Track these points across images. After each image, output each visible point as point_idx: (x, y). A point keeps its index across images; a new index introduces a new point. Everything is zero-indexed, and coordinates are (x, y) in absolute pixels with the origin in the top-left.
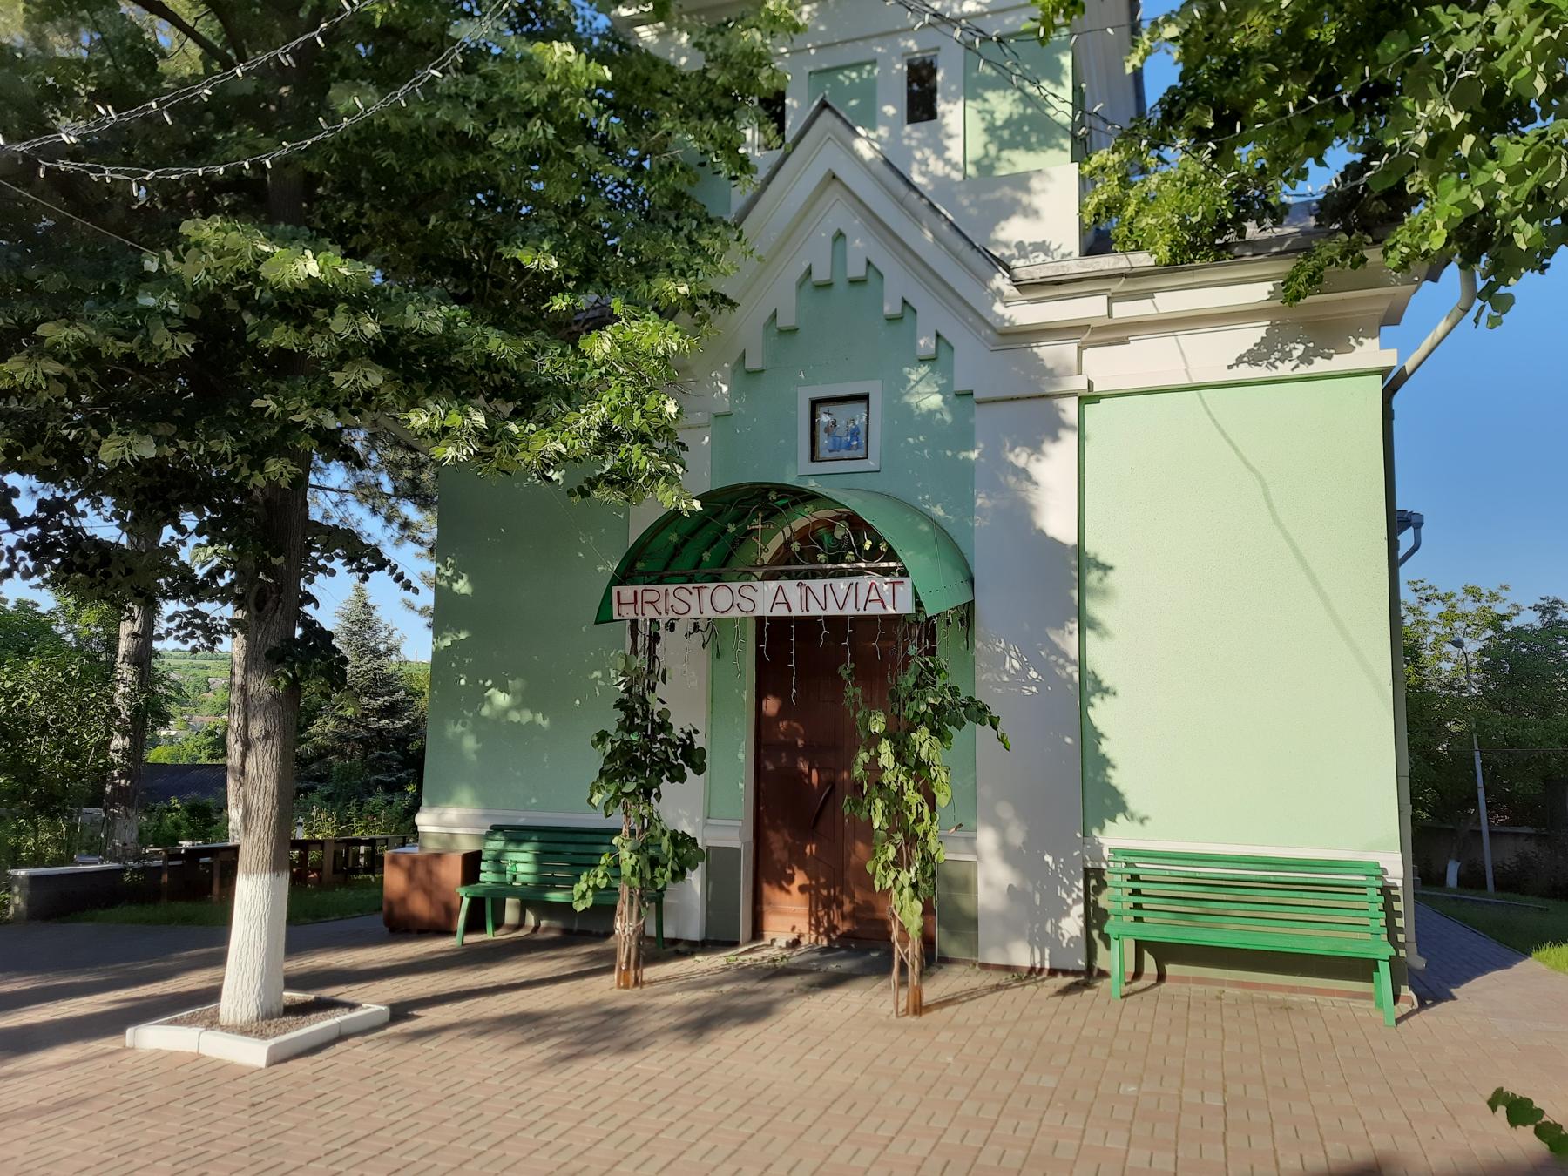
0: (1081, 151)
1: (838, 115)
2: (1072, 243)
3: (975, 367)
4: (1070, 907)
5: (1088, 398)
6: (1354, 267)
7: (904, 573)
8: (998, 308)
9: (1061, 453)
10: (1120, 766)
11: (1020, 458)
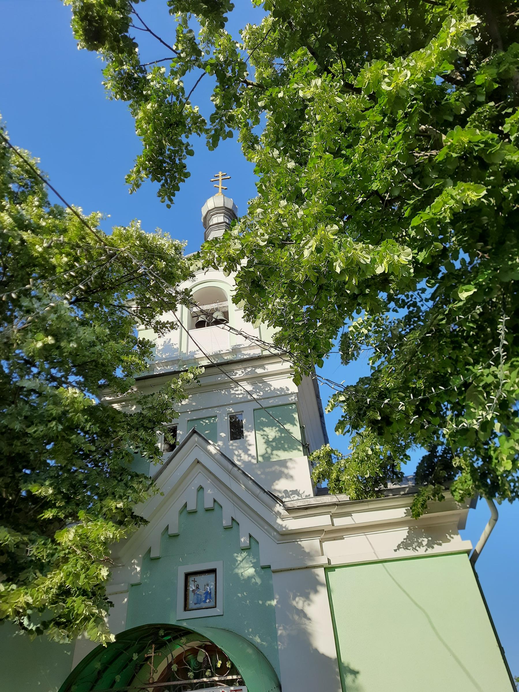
0: (307, 450)
1: (200, 436)
2: (309, 490)
3: (271, 553)
5: (329, 568)
6: (440, 500)
7: (242, 683)
8: (279, 521)
9: (320, 598)
11: (299, 603)
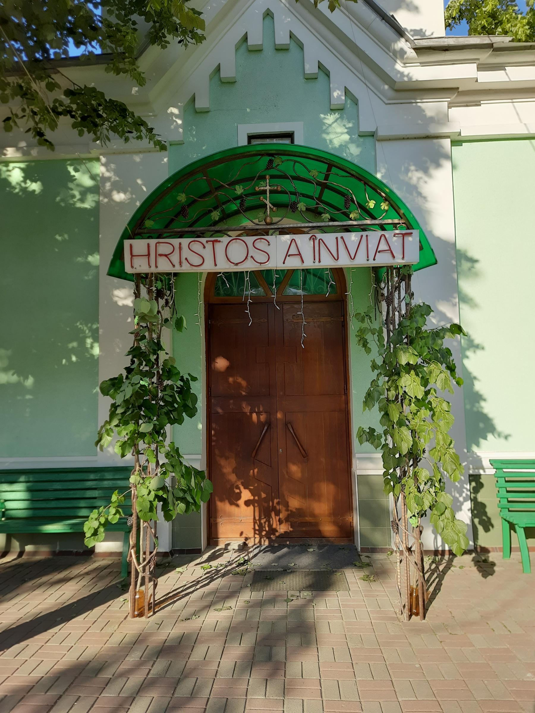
4: (462, 504)
8: (399, 66)
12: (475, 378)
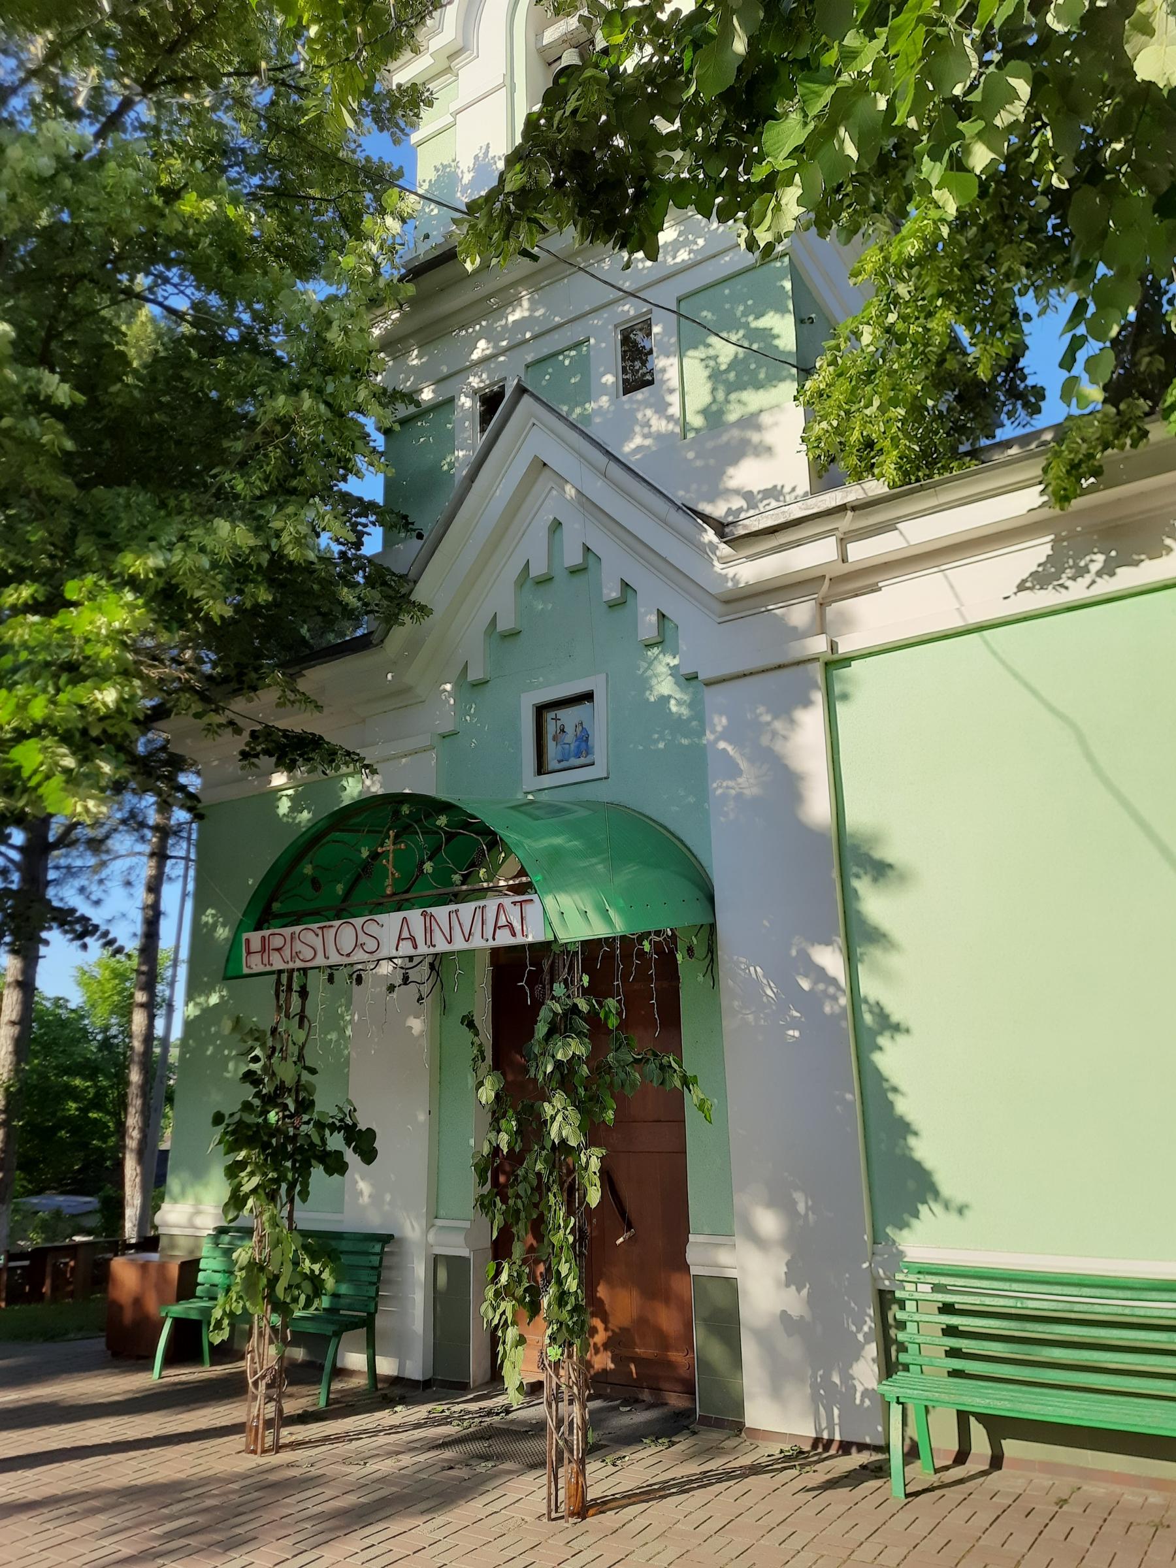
2: (803, 483)
4: (861, 1347)
10: (924, 1133)
12: (895, 1090)
